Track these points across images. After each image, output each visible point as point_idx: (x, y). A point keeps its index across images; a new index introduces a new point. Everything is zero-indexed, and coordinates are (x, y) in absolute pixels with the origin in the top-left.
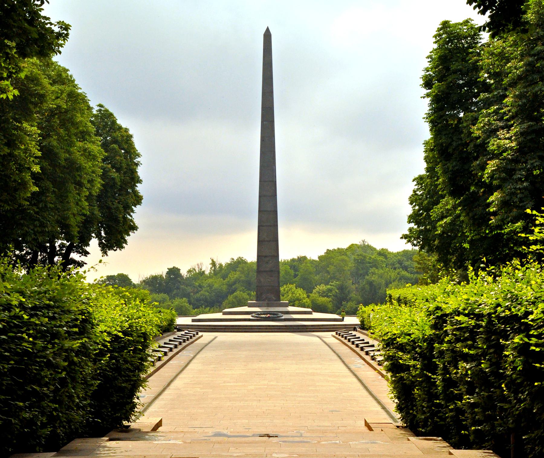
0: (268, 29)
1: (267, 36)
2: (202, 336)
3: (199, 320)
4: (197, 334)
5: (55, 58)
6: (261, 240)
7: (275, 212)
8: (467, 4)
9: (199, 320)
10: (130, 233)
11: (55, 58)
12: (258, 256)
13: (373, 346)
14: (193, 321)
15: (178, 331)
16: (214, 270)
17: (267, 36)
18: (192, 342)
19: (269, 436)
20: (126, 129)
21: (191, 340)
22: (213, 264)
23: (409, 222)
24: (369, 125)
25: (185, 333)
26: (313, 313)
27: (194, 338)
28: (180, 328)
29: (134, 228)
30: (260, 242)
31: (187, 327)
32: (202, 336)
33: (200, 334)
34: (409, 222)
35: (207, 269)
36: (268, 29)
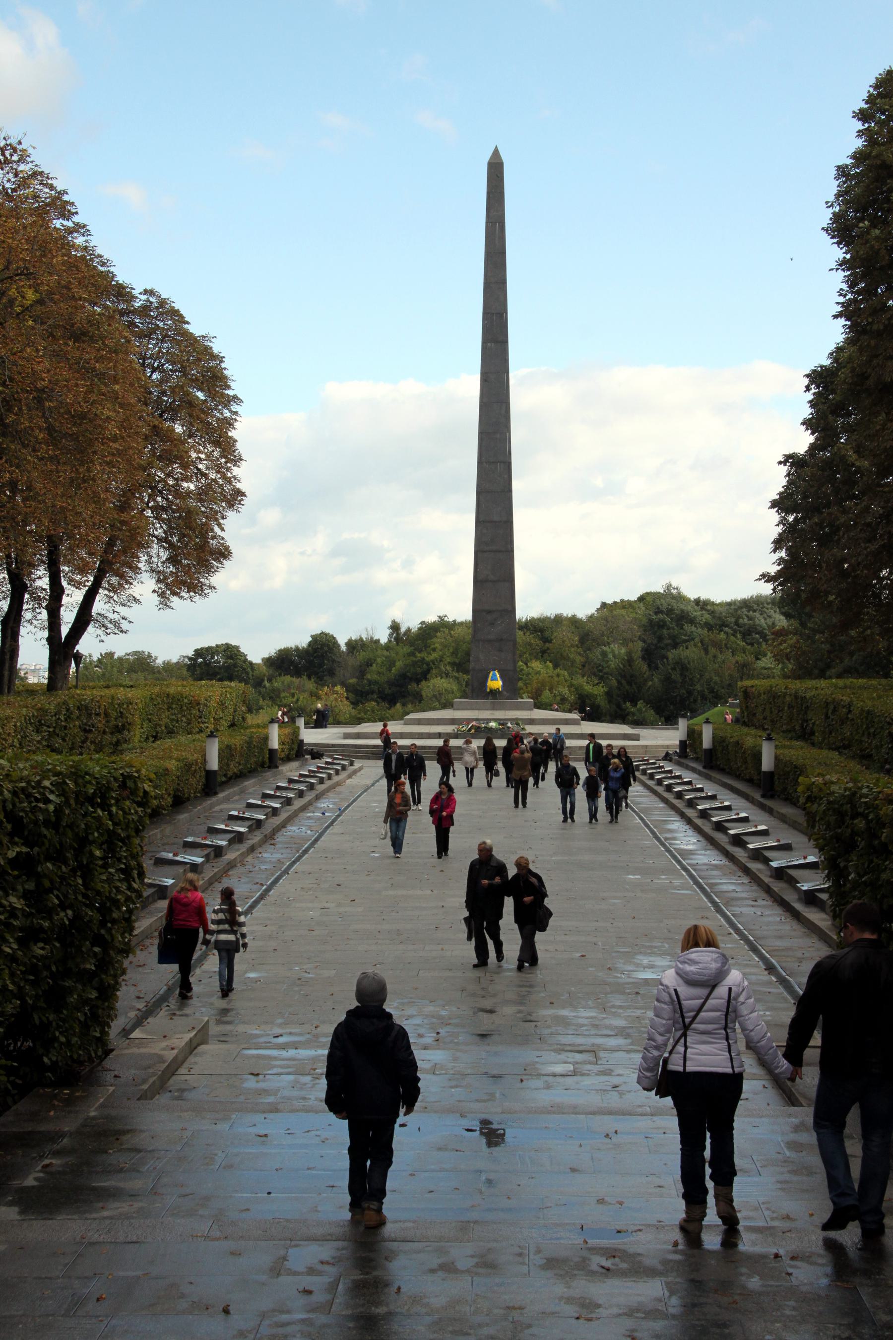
0: (496, 153)
1: (495, 170)
2: (361, 769)
3: (358, 736)
4: (352, 764)
7: (503, 282)
8: (803, 423)
9: (358, 736)
12: (475, 611)
13: (713, 797)
14: (347, 736)
15: (313, 758)
16: (396, 639)
20: (126, 777)
22: (395, 627)
24: (851, 1137)
25: (327, 763)
26: (582, 722)
30: (479, 582)
32: (361, 769)
33: (358, 764)
35: (383, 636)
36: (496, 153)
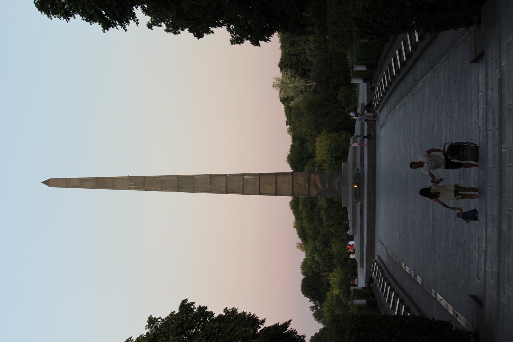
0: (43, 182)
1: (48, 183)
2: (378, 256)
4: (376, 261)
5: (290, 199)
6: (274, 192)
10: (288, 126)
11: (290, 199)
14: (362, 266)
15: (372, 282)
17: (48, 183)
18: (385, 266)
19: (486, 217)
21: (383, 268)
23: (146, 329)
27: (381, 265)
28: (370, 280)
29: (152, 321)
31: (368, 273)
32: (378, 256)
33: (376, 258)
34: (146, 329)
36: (43, 182)
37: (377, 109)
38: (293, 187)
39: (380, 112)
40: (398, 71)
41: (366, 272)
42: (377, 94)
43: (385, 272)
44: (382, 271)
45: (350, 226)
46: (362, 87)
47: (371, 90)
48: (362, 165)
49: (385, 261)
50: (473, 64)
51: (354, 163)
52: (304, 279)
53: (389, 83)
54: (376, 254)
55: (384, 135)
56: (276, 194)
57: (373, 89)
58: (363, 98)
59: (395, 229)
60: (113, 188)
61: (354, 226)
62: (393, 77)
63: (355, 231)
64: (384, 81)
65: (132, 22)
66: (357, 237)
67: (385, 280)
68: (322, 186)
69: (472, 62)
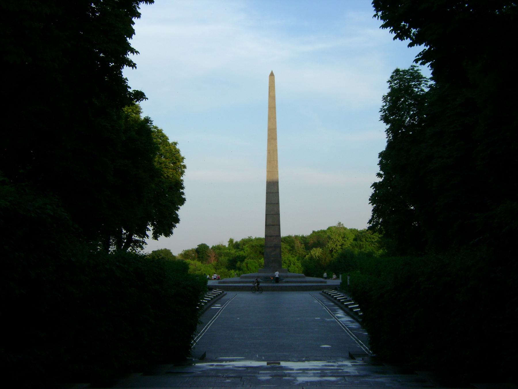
1: (272, 75)
2: (226, 294)
4: (223, 292)
14: (219, 283)
17: (272, 75)
18: (220, 298)
21: (219, 297)
27: (221, 296)
33: (225, 292)
37: (323, 292)
38: (271, 236)
39: (321, 294)
40: (347, 305)
41: (215, 286)
42: (332, 292)
43: (216, 298)
44: (217, 296)
45: (245, 275)
46: (338, 282)
47: (335, 288)
48: (287, 282)
49: (224, 298)
50: (348, 354)
51: (287, 277)
52: (208, 247)
53: (339, 300)
54: (228, 292)
55: (306, 296)
56: (266, 225)
57: (336, 289)
58: (330, 282)
59: (232, 307)
60: (269, 119)
61: (246, 277)
62: (343, 303)
63: (242, 278)
64: (340, 296)
65: (431, 76)
66: (237, 279)
67: (211, 298)
68: (269, 259)
69: (350, 353)
